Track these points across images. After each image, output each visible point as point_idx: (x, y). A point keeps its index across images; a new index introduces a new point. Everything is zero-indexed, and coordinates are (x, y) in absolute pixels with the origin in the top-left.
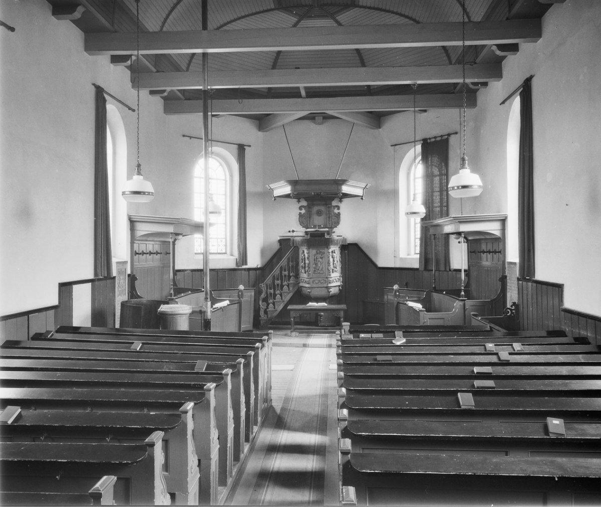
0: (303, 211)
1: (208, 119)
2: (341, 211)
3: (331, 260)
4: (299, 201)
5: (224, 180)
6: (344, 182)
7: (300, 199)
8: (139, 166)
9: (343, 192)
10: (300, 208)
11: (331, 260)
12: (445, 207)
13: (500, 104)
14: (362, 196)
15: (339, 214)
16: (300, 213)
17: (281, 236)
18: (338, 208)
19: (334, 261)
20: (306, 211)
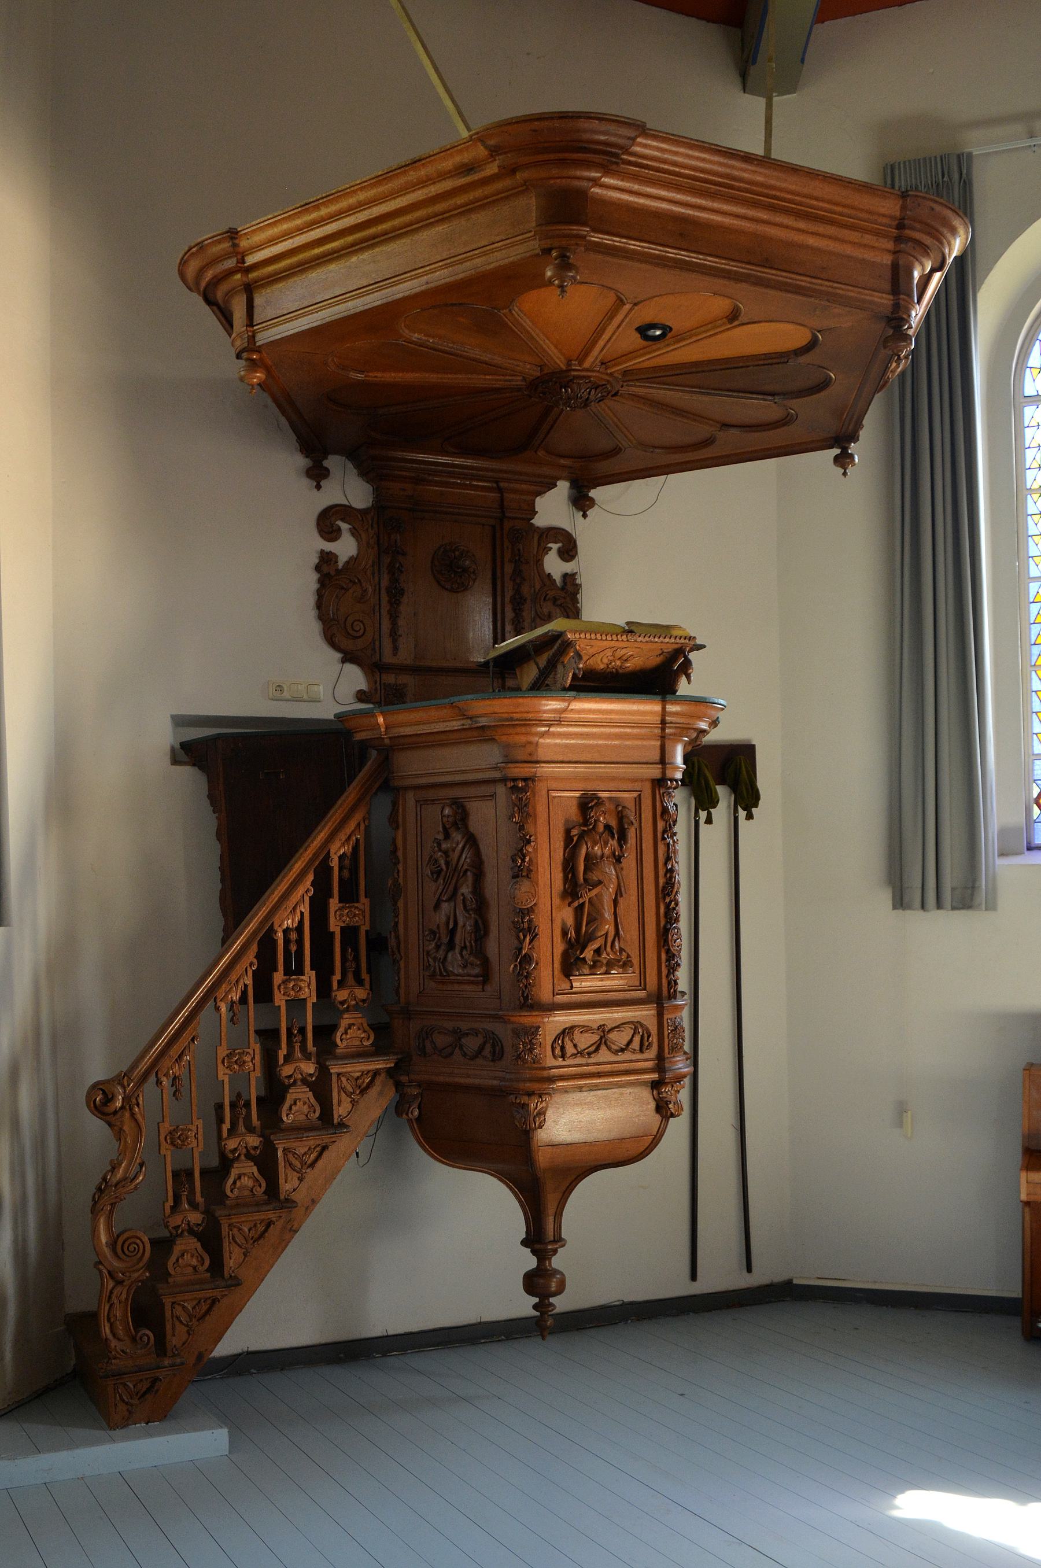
0: (346, 547)
2: (584, 565)
4: (317, 474)
10: (328, 523)
16: (326, 559)
18: (569, 550)
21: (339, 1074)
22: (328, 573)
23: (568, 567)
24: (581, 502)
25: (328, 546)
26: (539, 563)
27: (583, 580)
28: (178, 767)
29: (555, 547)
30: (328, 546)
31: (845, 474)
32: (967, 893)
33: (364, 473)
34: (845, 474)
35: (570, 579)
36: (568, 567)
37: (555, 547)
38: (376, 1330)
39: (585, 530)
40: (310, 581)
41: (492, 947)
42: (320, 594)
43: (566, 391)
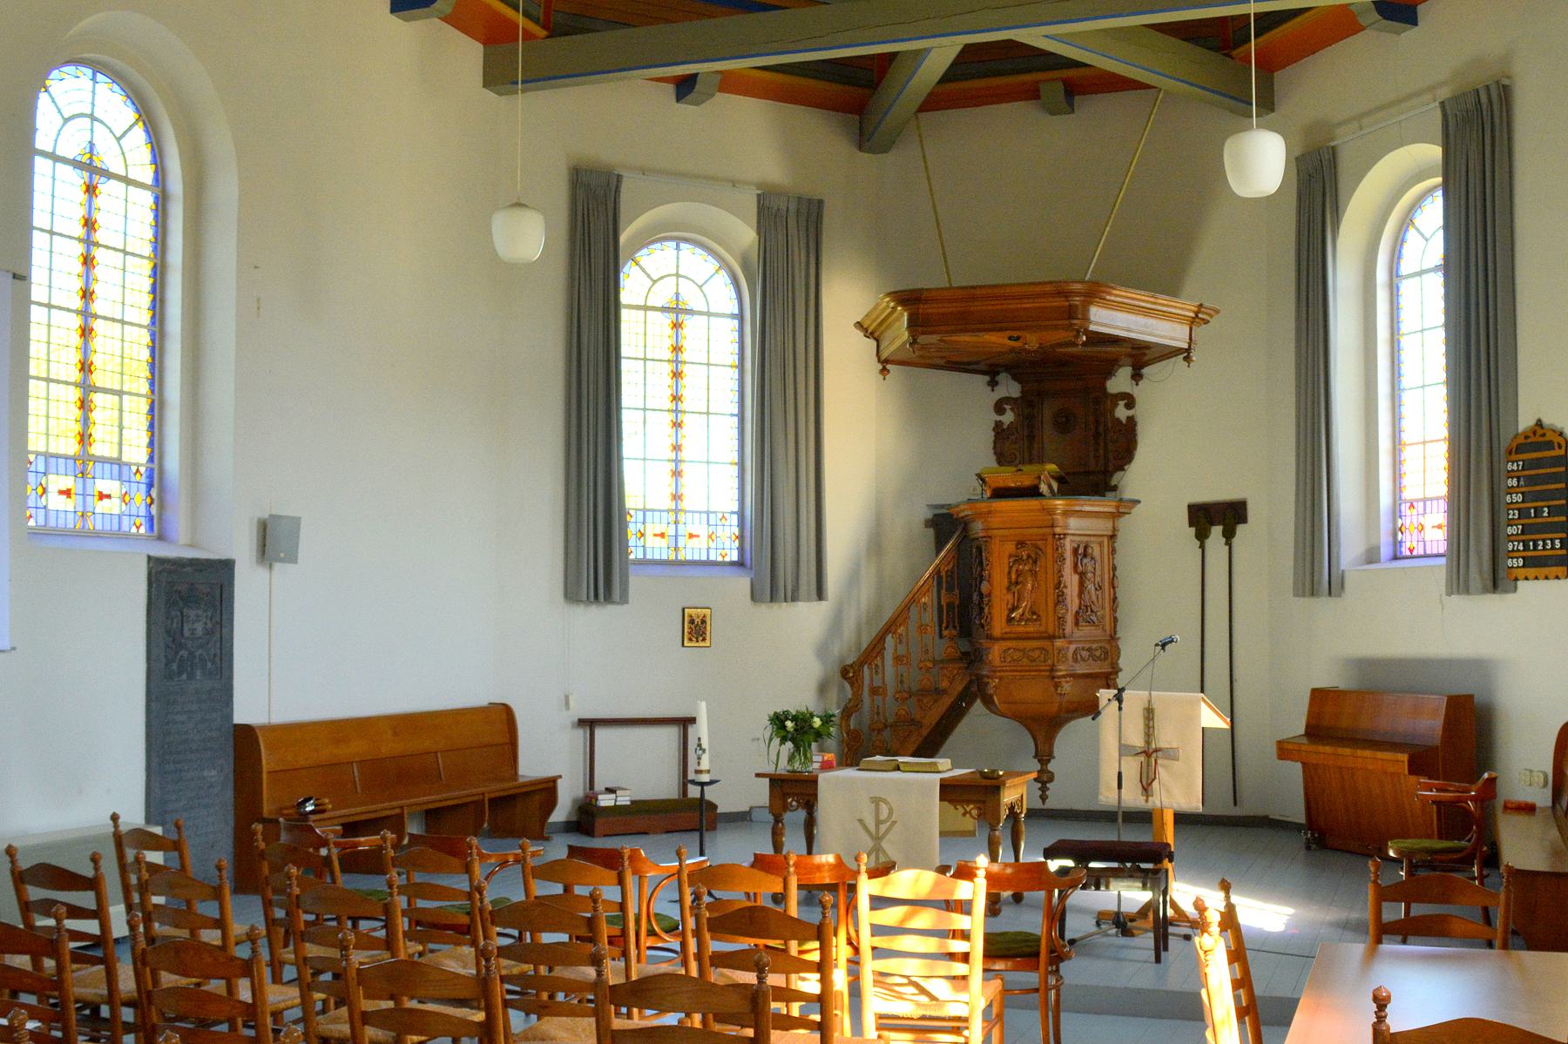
0: (1008, 418)
1: (816, 78)
2: (1139, 412)
3: (1071, 581)
4: (993, 384)
5: (733, 316)
6: (1094, 293)
7: (998, 373)
8: (15, 276)
9: (1092, 328)
10: (999, 408)
11: (1071, 581)
12: (296, 1022)
13: (1158, 960)
14: (1188, 350)
15: (1131, 421)
16: (998, 425)
17: (936, 507)
18: (1130, 402)
19: (1082, 584)
20: (1017, 415)
21: (1010, 620)
22: (998, 429)
23: (1130, 413)
24: (1137, 376)
25: (999, 418)
26: (1112, 412)
27: (1139, 419)
28: (223, 557)
29: (1122, 403)
30: (999, 418)
31: (115, 818)
32: (1335, 586)
33: (1015, 378)
34: (115, 818)
35: (1131, 420)
36: (1130, 413)
37: (1122, 403)
38: (1062, 1015)
39: (1140, 392)
40: (991, 436)
41: (1076, 578)
42: (995, 442)
43: (590, 1001)
